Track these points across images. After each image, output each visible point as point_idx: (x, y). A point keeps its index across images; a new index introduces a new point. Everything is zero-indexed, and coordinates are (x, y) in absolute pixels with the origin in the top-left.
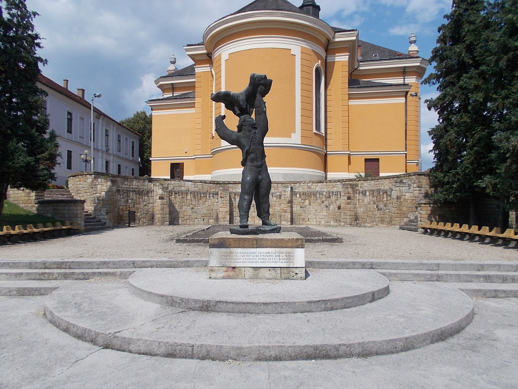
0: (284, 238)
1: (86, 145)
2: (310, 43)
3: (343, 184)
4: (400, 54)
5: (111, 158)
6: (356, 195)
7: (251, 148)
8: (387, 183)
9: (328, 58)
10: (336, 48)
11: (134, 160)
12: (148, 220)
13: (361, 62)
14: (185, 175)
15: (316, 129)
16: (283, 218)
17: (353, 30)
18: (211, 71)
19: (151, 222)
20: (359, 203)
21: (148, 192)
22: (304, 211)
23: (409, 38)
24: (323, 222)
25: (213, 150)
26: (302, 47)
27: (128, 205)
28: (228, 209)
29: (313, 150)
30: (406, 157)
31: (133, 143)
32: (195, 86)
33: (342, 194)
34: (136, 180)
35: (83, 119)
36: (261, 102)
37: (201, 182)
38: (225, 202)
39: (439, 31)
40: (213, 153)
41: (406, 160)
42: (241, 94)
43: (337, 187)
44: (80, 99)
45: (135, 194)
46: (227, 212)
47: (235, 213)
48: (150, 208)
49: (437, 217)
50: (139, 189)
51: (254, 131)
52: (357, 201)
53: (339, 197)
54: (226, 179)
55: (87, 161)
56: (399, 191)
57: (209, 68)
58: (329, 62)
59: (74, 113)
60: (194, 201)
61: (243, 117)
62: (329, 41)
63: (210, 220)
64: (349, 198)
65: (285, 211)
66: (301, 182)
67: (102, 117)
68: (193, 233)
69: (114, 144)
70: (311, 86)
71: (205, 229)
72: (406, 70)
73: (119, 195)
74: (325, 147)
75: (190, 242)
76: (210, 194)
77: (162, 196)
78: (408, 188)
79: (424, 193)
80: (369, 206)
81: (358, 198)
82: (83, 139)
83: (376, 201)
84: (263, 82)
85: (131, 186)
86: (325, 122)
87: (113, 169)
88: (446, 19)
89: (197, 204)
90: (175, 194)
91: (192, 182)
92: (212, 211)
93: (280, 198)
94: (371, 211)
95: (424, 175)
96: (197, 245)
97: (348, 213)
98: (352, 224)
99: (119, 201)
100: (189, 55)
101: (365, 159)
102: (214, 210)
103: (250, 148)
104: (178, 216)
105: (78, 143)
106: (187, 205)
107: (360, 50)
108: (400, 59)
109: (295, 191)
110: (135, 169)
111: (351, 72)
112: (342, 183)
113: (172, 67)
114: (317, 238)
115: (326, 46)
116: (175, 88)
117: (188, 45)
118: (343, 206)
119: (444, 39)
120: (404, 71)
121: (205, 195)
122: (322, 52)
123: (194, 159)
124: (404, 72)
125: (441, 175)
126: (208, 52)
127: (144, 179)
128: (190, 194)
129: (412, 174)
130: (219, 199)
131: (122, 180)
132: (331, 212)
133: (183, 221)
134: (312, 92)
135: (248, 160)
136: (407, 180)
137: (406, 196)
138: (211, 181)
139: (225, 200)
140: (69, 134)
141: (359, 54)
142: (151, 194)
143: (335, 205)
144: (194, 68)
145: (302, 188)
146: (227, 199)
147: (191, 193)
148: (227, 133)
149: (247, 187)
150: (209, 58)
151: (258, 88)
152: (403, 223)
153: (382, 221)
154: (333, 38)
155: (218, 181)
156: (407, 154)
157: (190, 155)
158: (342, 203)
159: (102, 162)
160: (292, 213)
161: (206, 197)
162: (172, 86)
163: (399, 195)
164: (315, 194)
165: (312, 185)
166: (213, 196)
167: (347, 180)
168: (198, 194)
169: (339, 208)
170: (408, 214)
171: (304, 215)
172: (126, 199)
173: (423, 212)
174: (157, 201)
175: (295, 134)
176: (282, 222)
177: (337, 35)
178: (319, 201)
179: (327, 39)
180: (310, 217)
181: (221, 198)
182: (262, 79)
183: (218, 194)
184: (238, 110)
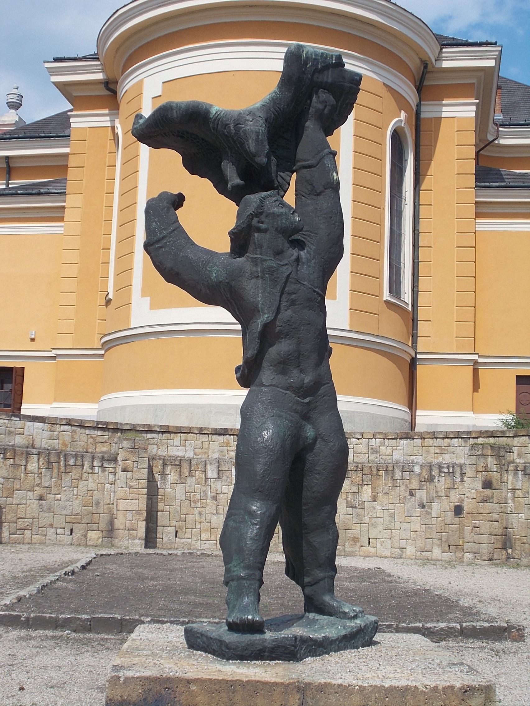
0: (414, 684)
6: (506, 475)
7: (279, 317)
9: (423, 109)
13: (502, 125)
15: (390, 292)
17: (487, 44)
18: (113, 128)
20: (513, 500)
22: (358, 516)
24: (410, 550)
25: (106, 335)
29: (387, 350)
32: (68, 165)
33: (469, 472)
36: (322, 150)
37: (69, 422)
40: (108, 346)
42: (250, 113)
43: (453, 452)
46: (138, 512)
51: (296, 254)
52: (510, 495)
53: (459, 480)
54: (139, 419)
57: (108, 118)
58: (425, 118)
61: (254, 199)
62: (426, 67)
63: (93, 535)
64: (488, 485)
68: (38, 585)
71: (76, 570)
74: (413, 342)
75: (28, 624)
76: (93, 458)
81: (512, 484)
84: (329, 77)
86: (413, 275)
89: (55, 486)
91: (44, 422)
96: (54, 638)
97: (485, 527)
98: (496, 557)
100: (57, 85)
101: (516, 376)
102: (101, 504)
103: (276, 317)
106: (27, 487)
112: (466, 442)
114: (443, 625)
115: (418, 77)
117: (57, 60)
118: (470, 506)
121: (79, 462)
126: (109, 79)
128: (35, 457)
130: (120, 473)
132: (434, 521)
133: (13, 530)
134: (381, 192)
135: (265, 364)
138: (98, 423)
141: (498, 108)
144: (69, 118)
147: (39, 454)
148: (191, 256)
149: (259, 468)
150: (108, 93)
151: (311, 98)
154: (436, 60)
158: (468, 498)
161: (83, 466)
162: (8, 163)
164: (391, 469)
165: (382, 444)
166: (102, 466)
167: (481, 432)
168: (59, 458)
169: (458, 510)
171: (358, 527)
177: (446, 52)
178: (401, 490)
179: (421, 59)
181: (125, 470)
182: (328, 67)
183: (115, 460)
184: (235, 175)
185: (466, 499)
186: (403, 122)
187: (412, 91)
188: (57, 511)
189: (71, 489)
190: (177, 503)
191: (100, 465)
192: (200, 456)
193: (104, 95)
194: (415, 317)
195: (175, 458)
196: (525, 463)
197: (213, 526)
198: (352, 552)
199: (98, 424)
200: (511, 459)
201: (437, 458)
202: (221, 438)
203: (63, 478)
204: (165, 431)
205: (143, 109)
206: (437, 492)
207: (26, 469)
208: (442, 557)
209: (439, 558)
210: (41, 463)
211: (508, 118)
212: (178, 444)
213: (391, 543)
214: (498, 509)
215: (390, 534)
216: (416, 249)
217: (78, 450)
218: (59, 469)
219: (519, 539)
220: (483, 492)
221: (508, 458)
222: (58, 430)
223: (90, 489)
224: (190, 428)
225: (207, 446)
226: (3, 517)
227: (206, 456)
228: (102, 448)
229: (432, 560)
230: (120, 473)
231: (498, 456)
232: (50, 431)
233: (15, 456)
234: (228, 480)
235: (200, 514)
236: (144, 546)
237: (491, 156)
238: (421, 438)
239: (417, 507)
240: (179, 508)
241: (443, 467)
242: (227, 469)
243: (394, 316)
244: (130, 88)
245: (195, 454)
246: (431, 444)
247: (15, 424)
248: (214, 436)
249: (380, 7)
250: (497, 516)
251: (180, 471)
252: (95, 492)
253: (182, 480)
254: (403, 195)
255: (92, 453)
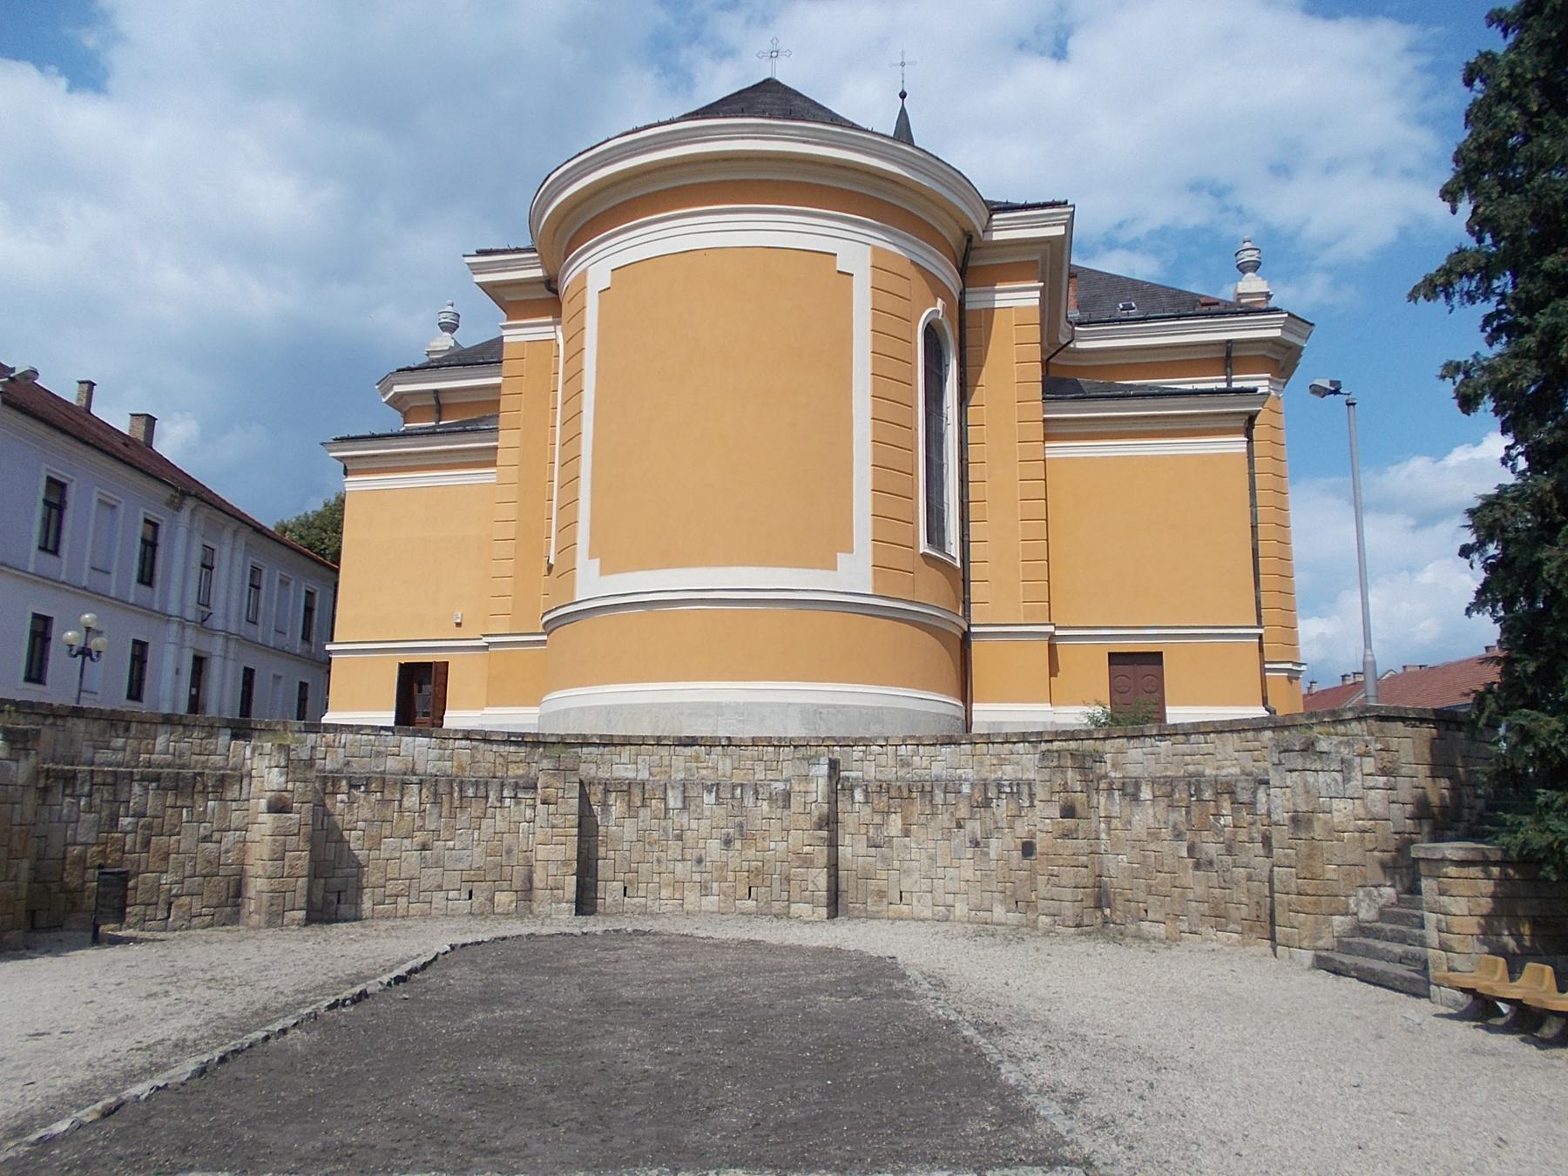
1: (135, 605)
2: (905, 238)
3: (1043, 753)
4: (1208, 302)
5: (215, 647)
6: (1095, 796)
8: (1230, 750)
9: (968, 298)
10: (991, 265)
11: (309, 652)
12: (215, 901)
13: (1079, 324)
14: (450, 709)
16: (798, 890)
19: (229, 909)
20: (1108, 834)
21: (226, 781)
22: (884, 858)
23: (1236, 254)
24: (960, 909)
26: (875, 249)
27: (118, 839)
28: (569, 849)
30: (1261, 649)
31: (310, 595)
33: (1041, 793)
34: (168, 728)
35: (114, 507)
38: (558, 821)
39: (1469, 82)
40: (550, 627)
41: (1263, 662)
43: (1018, 763)
44: (126, 445)
45: (158, 788)
46: (565, 863)
47: (603, 867)
48: (227, 851)
49: (1526, 929)
50: (183, 766)
53: (1027, 804)
55: (90, 654)
56: (1300, 790)
59: (74, 484)
60: (435, 816)
62: (970, 240)
63: (500, 897)
64: (1069, 812)
65: (807, 862)
66: (869, 739)
67: (190, 503)
69: (235, 596)
70: (911, 384)
72: (1233, 354)
73: (71, 796)
74: (964, 610)
76: (502, 785)
77: (279, 799)
78: (1339, 777)
79: (1409, 799)
80: (1153, 846)
81: (1106, 809)
82: (107, 576)
83: (1183, 828)
85: (143, 757)
87: (223, 684)
88: (1496, 32)
90: (352, 786)
92: (509, 859)
93: (787, 805)
94: (1166, 869)
95: (1403, 719)
97: (1068, 876)
98: (1086, 921)
99: (67, 823)
100: (483, 286)
101: (1109, 654)
104: (360, 880)
105: (85, 588)
106: (403, 832)
107: (1074, 290)
108: (1212, 315)
109: (848, 778)
110: (310, 684)
111: (1046, 358)
112: (1036, 748)
113: (444, 342)
115: (960, 256)
116: (444, 405)
117: (481, 253)
118: (1044, 844)
119: (1515, 92)
120: (1228, 356)
121: (482, 792)
122: (952, 278)
123: (485, 648)
124: (1229, 357)
125: (1548, 723)
127: (211, 726)
128: (415, 788)
129: (1349, 715)
130: (539, 806)
131: (96, 728)
132: (993, 865)
133: (377, 899)
134: (912, 406)
136: (1336, 739)
137: (1335, 813)
138: (510, 734)
139: (561, 811)
140: (49, 558)
141: (1072, 302)
142: (237, 787)
143: (1008, 838)
145: (877, 766)
146: (568, 810)
147: (421, 783)
150: (551, 295)
152: (1327, 941)
153: (1218, 917)
154: (984, 231)
155: (537, 735)
156: (1264, 640)
157: (473, 634)
159: (179, 659)
160: (833, 867)
161: (487, 797)
163: (1305, 809)
165: (916, 753)
166: (515, 797)
168: (452, 788)
169: (1028, 849)
170: (1347, 896)
172: (104, 814)
173: (1458, 906)
174: (259, 820)
175: (848, 555)
176: (793, 906)
178: (944, 819)
179: (963, 230)
180: (906, 885)
183: (535, 787)
185: (1038, 833)
186: (941, 314)
187: (956, 277)
188: (448, 865)
189: (470, 831)
190: (626, 846)
191: (512, 795)
192: (658, 778)
193: (547, 299)
194: (966, 576)
195: (620, 781)
196: (1123, 777)
197: (677, 879)
198: (878, 912)
199: (509, 737)
200: (1103, 772)
201: (995, 772)
202: (688, 751)
203: (458, 816)
204: (608, 742)
205: (588, 308)
206: (996, 822)
207: (400, 806)
208: (1007, 919)
209: (1003, 921)
210: (424, 796)
211: (1087, 314)
212: (627, 761)
213: (933, 898)
214: (1086, 847)
215: (930, 885)
216: (965, 484)
217: (481, 774)
218: (451, 803)
219: (1121, 894)
220: (1063, 823)
221: (1098, 771)
222: (451, 747)
223: (497, 830)
224: (644, 737)
225: (668, 763)
226: (364, 880)
227: (667, 777)
228: (516, 771)
229: (992, 923)
230: (539, 806)
231: (1082, 768)
232: (440, 748)
233: (384, 788)
234: (699, 811)
235: (659, 861)
236: (574, 912)
237: (1066, 366)
238: (971, 743)
239: (968, 845)
240: (628, 853)
241: (1003, 786)
242: (696, 795)
243: (936, 575)
244: (571, 283)
245: (651, 774)
246: (985, 752)
247: (385, 741)
248: (677, 748)
249: (904, 156)
250: (1085, 858)
251: (629, 800)
252: (505, 835)
253: (631, 810)
254: (944, 411)
255: (502, 778)
